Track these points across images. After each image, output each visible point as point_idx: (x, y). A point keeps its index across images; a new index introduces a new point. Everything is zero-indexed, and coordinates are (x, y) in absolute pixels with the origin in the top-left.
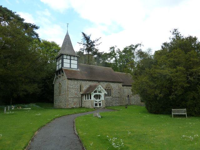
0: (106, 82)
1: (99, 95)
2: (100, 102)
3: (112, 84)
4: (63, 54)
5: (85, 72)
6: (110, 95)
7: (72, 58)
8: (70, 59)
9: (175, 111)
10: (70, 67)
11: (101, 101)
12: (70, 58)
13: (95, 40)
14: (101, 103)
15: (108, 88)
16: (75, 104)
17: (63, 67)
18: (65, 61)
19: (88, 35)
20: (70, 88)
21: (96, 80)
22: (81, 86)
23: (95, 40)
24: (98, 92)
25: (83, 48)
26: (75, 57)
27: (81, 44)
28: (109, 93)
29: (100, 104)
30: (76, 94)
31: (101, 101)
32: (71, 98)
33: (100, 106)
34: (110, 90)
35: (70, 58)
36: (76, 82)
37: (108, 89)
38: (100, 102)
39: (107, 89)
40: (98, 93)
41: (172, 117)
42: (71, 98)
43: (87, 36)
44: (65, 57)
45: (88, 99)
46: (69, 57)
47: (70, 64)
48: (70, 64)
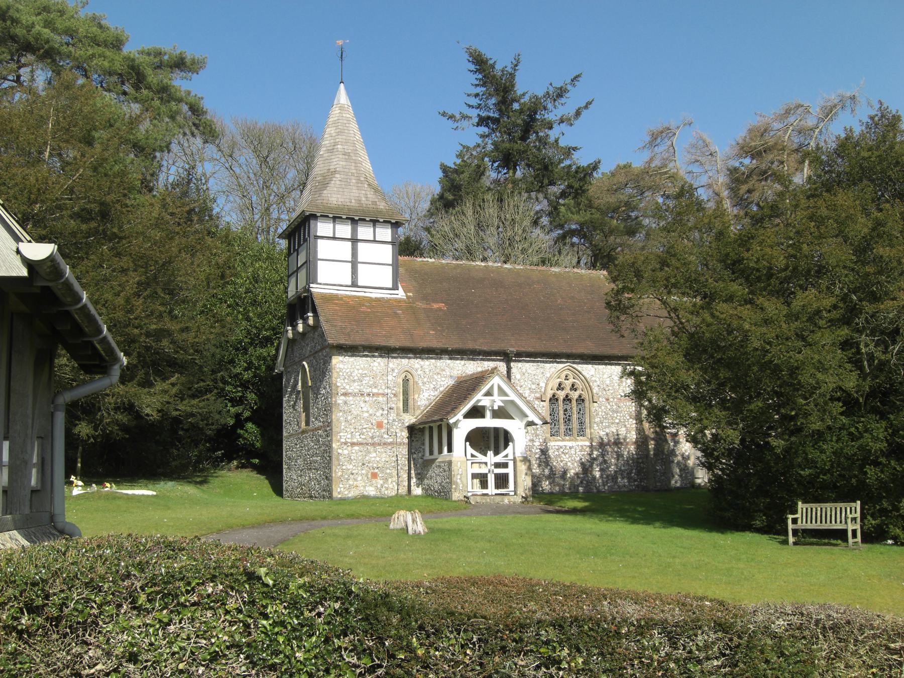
0: (553, 357)
1: (496, 430)
2: (505, 465)
3: (589, 370)
4: (314, 217)
5: (435, 306)
6: (581, 432)
7: (365, 232)
8: (354, 240)
9: (174, 476)
10: (354, 284)
11: (511, 464)
12: (354, 231)
13: (540, 94)
14: (510, 470)
15: (567, 390)
16: (374, 476)
17: (315, 281)
18: (324, 249)
19: (501, 62)
20: (345, 394)
21: (495, 347)
22: (406, 381)
23: (540, 94)
24: (488, 414)
25: (480, 141)
26: (338, 227)
27: (465, 123)
28: (575, 416)
29: (501, 481)
30: (380, 425)
31: (511, 464)
32: (353, 444)
33: (485, 491)
34: (580, 400)
35: (354, 231)
36: (378, 363)
37: (567, 399)
38: (505, 465)
39: (561, 395)
40: (488, 422)
41: (785, 542)
42: (353, 444)
43: (498, 67)
44: (323, 228)
45: (440, 452)
46: (345, 230)
47: (354, 263)
48: (354, 263)
